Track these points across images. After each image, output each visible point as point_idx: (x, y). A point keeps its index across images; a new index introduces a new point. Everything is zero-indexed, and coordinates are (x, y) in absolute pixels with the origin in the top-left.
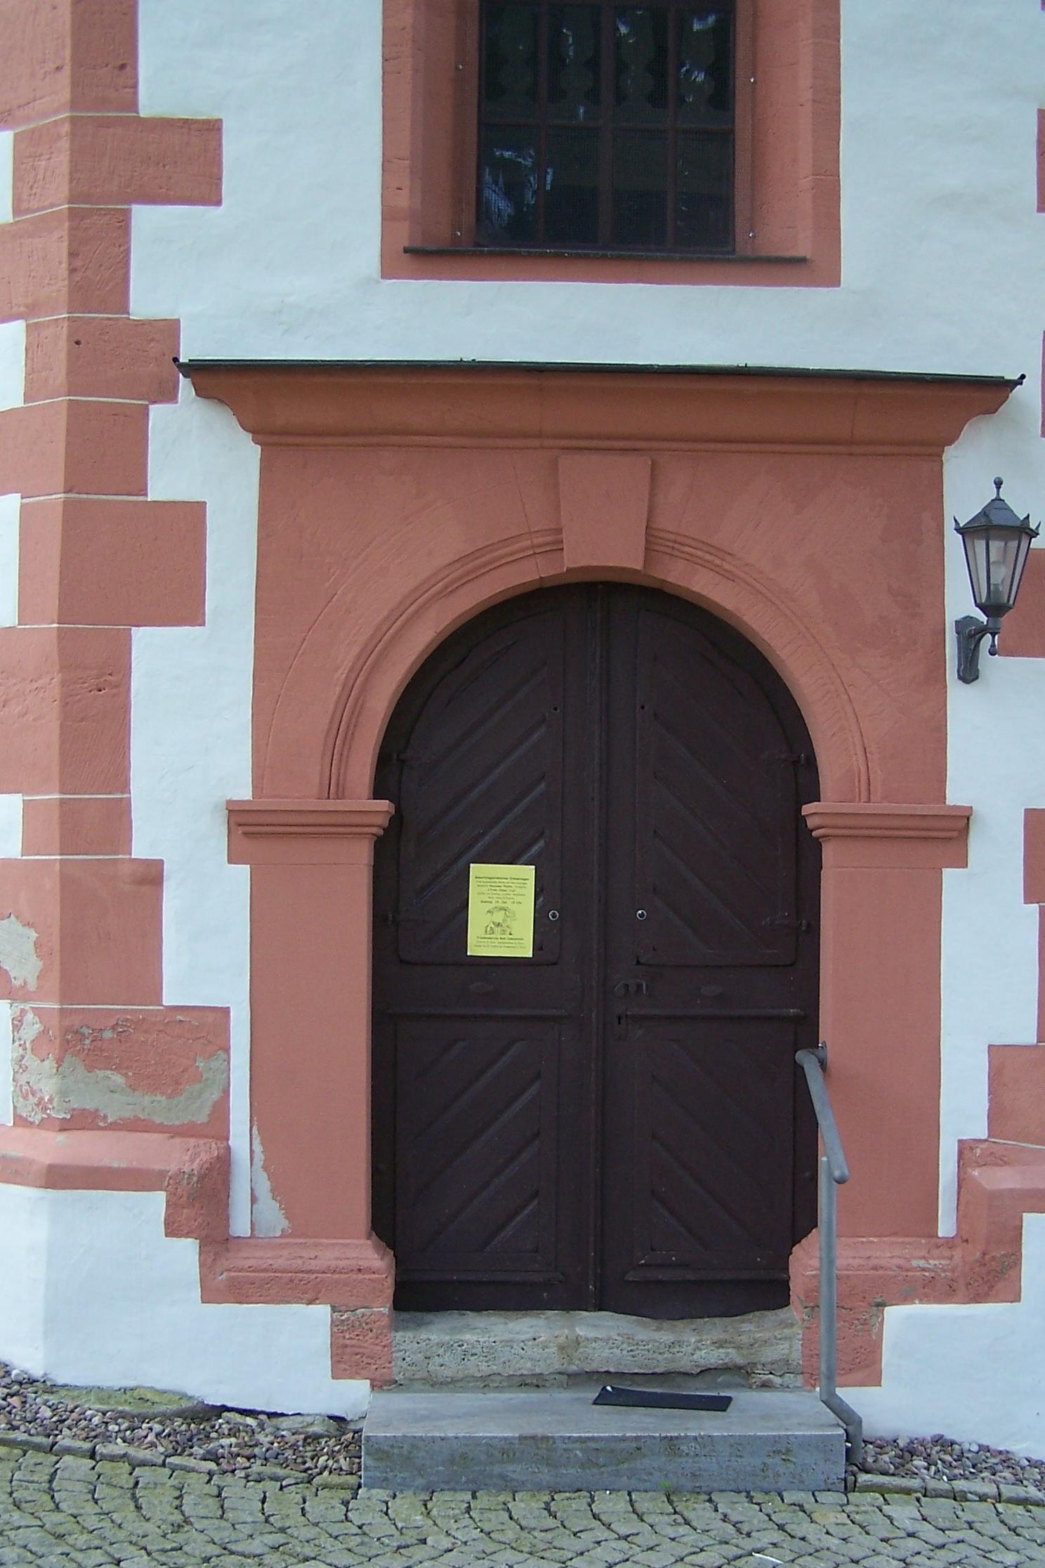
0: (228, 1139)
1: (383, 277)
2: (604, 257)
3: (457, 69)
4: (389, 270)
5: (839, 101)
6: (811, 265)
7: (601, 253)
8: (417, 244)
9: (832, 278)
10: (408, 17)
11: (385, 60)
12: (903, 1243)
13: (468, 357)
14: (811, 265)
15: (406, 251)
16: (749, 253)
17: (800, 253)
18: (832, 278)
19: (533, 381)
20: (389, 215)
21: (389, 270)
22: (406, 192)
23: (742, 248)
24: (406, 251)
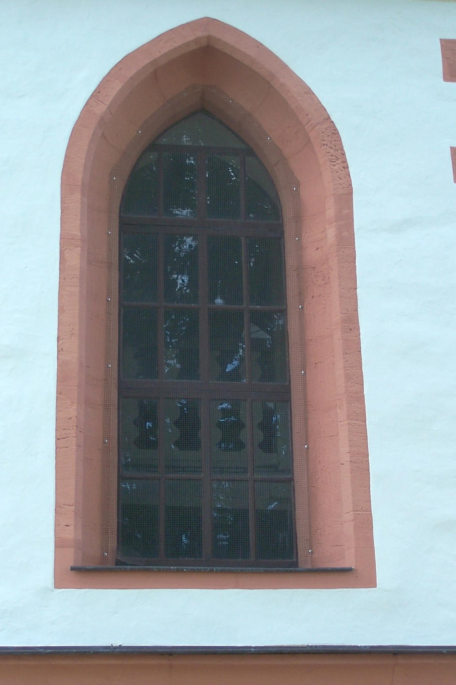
0: (329, 118)
1: (55, 588)
2: (212, 571)
3: (104, 442)
4: (59, 583)
5: (368, 461)
6: (354, 573)
7: (209, 568)
8: (79, 565)
9: (370, 581)
10: (73, 411)
11: (57, 439)
12: (192, 569)
13: (116, 643)
14: (354, 573)
15: (72, 569)
16: (309, 566)
17: (347, 565)
18: (370, 581)
19: (164, 662)
20: (60, 544)
21: (59, 583)
22: (72, 528)
23: (304, 563)
24: (72, 569)
